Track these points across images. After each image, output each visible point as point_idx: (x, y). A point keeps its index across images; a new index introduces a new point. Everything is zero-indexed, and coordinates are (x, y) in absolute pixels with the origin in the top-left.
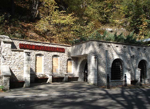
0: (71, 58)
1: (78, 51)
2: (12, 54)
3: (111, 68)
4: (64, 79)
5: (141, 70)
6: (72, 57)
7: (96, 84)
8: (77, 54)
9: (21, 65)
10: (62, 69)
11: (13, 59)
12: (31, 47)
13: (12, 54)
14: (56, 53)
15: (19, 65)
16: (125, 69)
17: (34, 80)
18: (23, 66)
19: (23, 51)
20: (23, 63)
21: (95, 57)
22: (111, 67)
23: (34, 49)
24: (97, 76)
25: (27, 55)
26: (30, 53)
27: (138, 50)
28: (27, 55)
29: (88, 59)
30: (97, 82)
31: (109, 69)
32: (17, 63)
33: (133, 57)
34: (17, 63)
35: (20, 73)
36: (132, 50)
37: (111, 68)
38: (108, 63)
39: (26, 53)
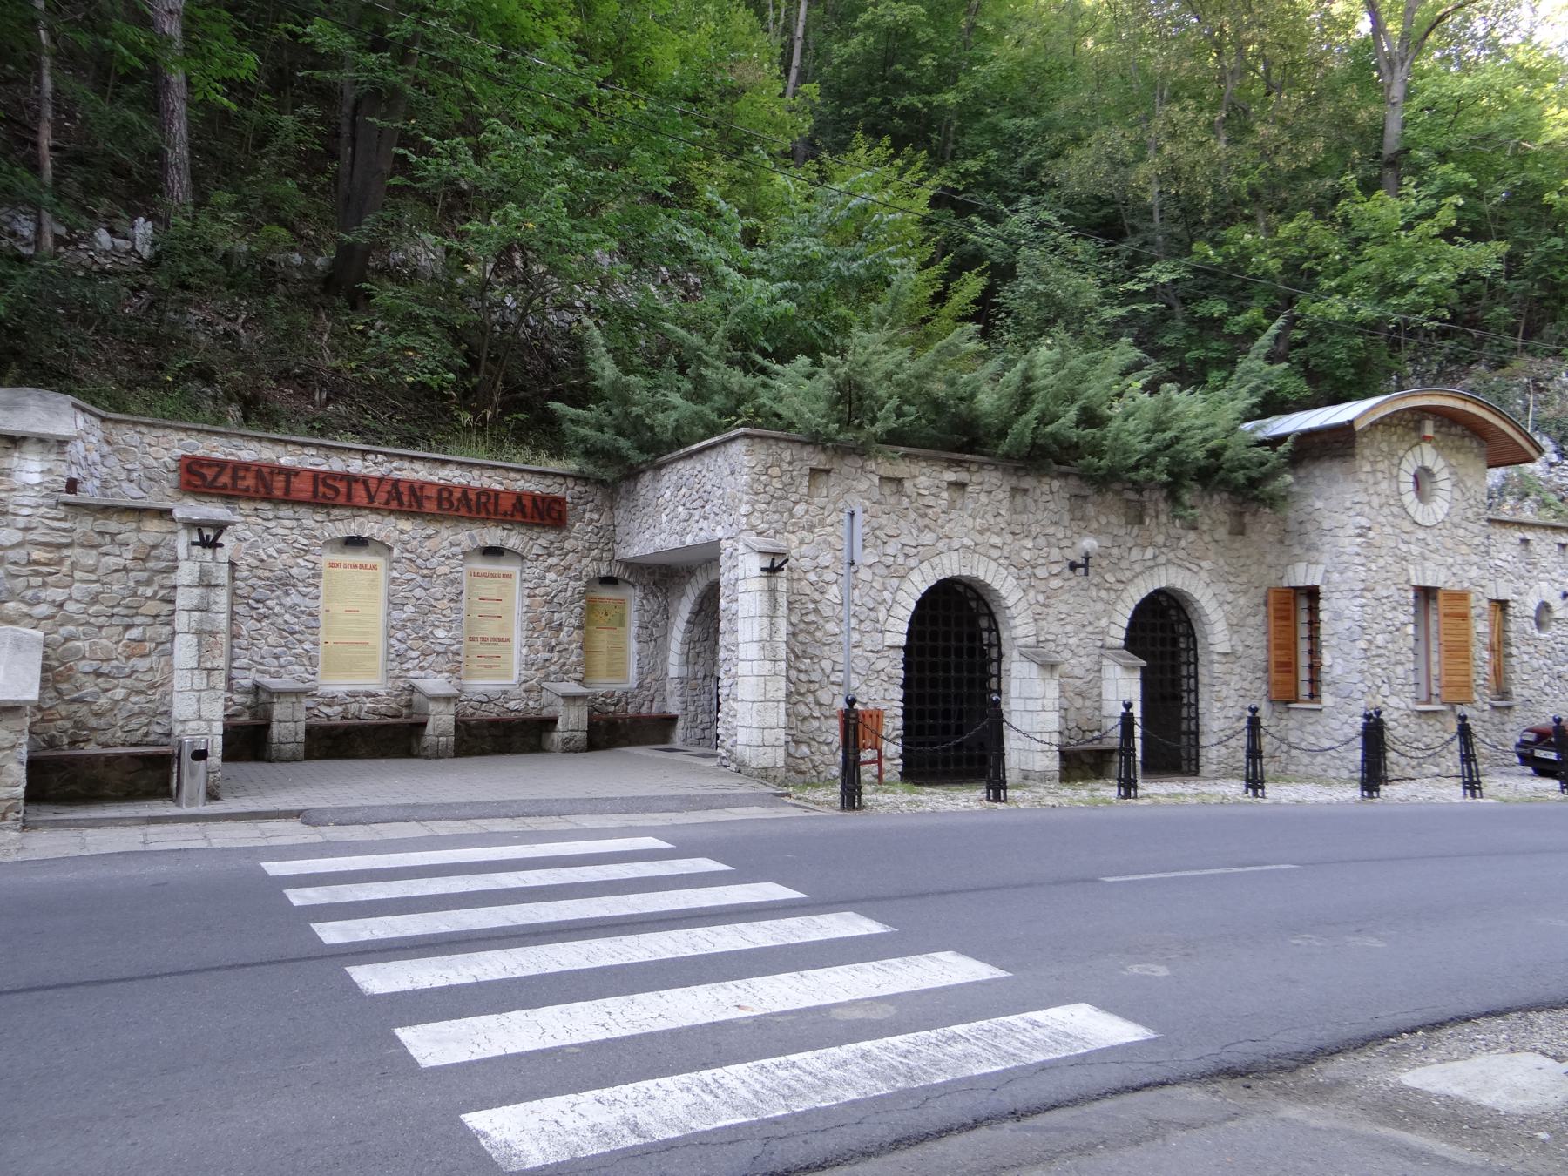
0: (617, 571)
1: (664, 518)
2: (75, 536)
3: (902, 654)
4: (556, 737)
5: (1144, 663)
6: (629, 564)
7: (772, 774)
8: (657, 539)
9: (149, 621)
10: (547, 655)
11: (78, 575)
12: (279, 483)
13: (75, 536)
14: (493, 536)
15: (138, 620)
16: (1015, 655)
17: (302, 736)
18: (167, 630)
19: (169, 511)
20: (170, 607)
21: (768, 565)
22: (902, 640)
23: (307, 495)
24: (782, 705)
25: (194, 544)
26: (220, 527)
27: (1290, 493)
28: (194, 544)
29: (723, 581)
30: (781, 752)
31: (891, 653)
32: (115, 610)
33: (1086, 566)
34: (115, 610)
35: (141, 686)
36: (1078, 514)
37: (905, 648)
38: (882, 609)
39: (190, 525)
